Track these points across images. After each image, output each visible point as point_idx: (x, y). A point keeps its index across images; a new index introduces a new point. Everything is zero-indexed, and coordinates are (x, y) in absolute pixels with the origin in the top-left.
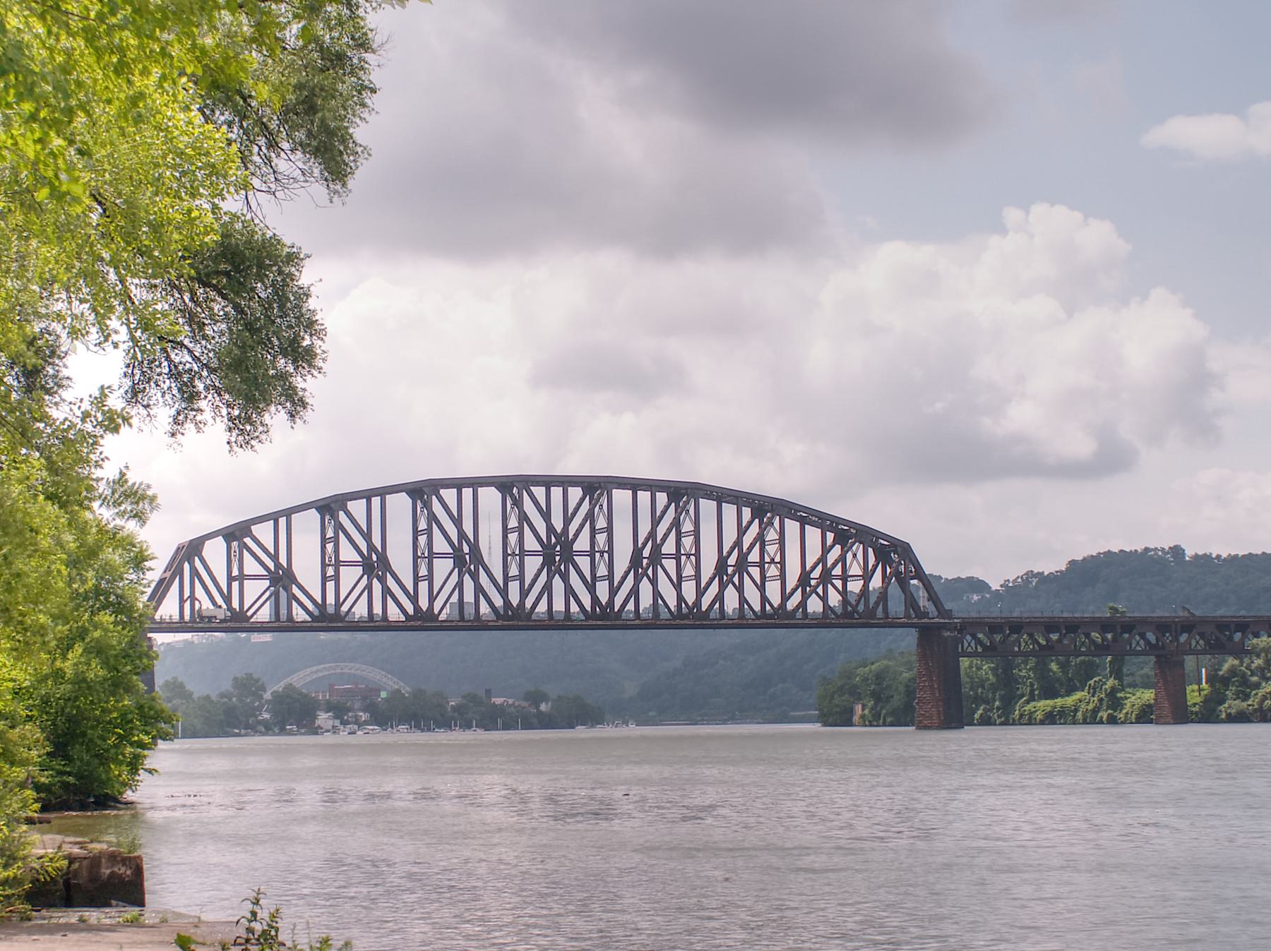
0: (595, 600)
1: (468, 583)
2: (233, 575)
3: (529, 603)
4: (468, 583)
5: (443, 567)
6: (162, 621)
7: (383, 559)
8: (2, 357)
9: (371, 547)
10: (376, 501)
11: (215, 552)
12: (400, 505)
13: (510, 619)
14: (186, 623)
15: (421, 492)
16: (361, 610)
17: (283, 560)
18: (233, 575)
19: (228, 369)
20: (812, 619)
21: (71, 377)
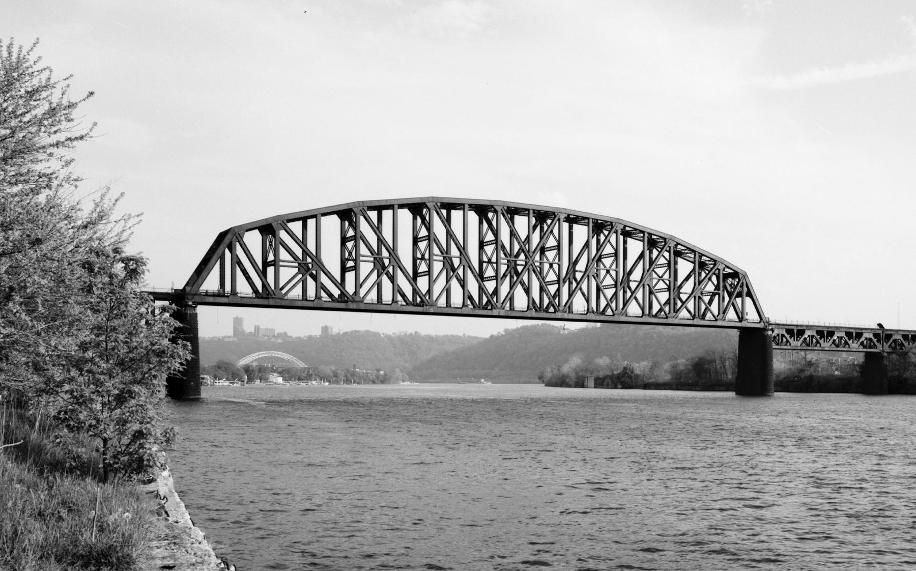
0: (415, 292)
1: (311, 284)
2: (269, 260)
3: (362, 292)
4: (311, 284)
5: (366, 267)
6: (207, 294)
7: (317, 259)
8: (195, 570)
9: (306, 252)
10: (311, 223)
11: (254, 240)
12: (332, 226)
13: (485, 308)
14: (228, 297)
15: (346, 214)
16: (296, 293)
17: (311, 246)
18: (269, 260)
19: (51, 473)
20: (681, 319)
21: (150, 270)
